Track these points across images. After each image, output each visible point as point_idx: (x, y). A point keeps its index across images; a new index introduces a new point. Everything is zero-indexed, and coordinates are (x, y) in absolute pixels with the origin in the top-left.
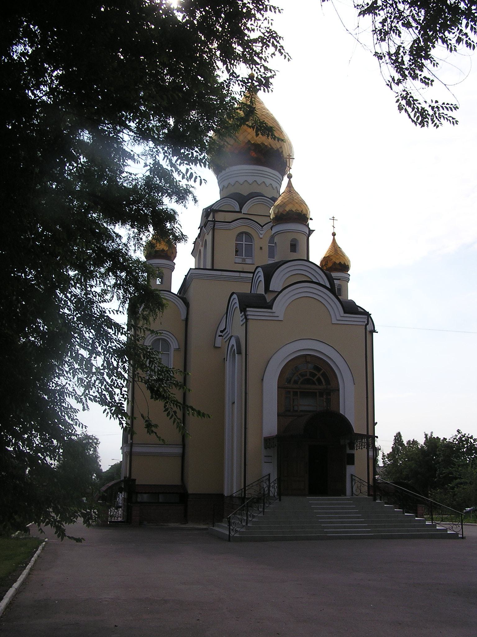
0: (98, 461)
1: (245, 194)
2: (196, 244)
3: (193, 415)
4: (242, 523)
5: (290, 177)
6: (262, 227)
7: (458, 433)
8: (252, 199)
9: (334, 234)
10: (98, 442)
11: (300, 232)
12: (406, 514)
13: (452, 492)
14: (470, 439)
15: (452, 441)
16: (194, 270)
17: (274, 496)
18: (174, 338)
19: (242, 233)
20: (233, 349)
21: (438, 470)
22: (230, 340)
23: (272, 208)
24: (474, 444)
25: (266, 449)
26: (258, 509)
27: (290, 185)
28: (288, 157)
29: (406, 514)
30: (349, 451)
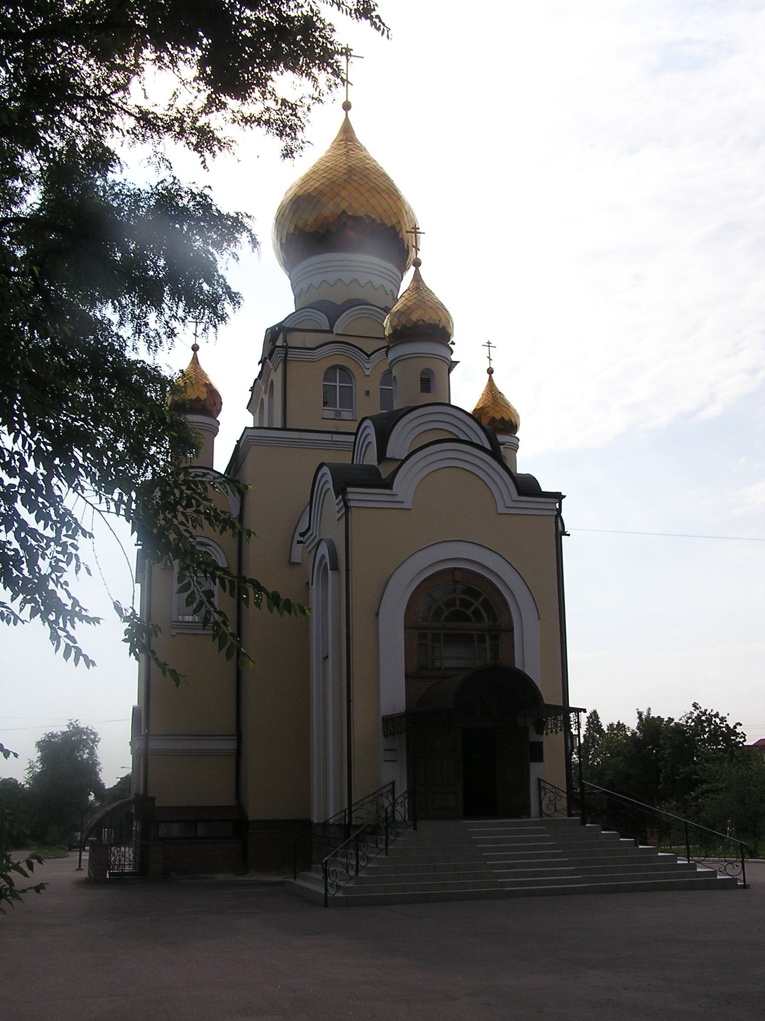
0: (98, 770)
1: (339, 301)
2: (255, 390)
3: (258, 605)
4: (348, 872)
5: (417, 264)
6: (369, 356)
7: (694, 708)
8: (351, 310)
9: (490, 371)
10: (97, 739)
11: (434, 356)
12: (640, 847)
13: (695, 806)
14: (715, 718)
15: (685, 723)
16: (252, 430)
17: (405, 821)
18: (219, 550)
19: (334, 367)
20: (324, 563)
21: (664, 770)
22: (316, 551)
23: (387, 317)
24: (722, 725)
25: (387, 736)
26: (377, 846)
27: (417, 277)
28: (413, 230)
29: (640, 847)
30: (533, 737)
